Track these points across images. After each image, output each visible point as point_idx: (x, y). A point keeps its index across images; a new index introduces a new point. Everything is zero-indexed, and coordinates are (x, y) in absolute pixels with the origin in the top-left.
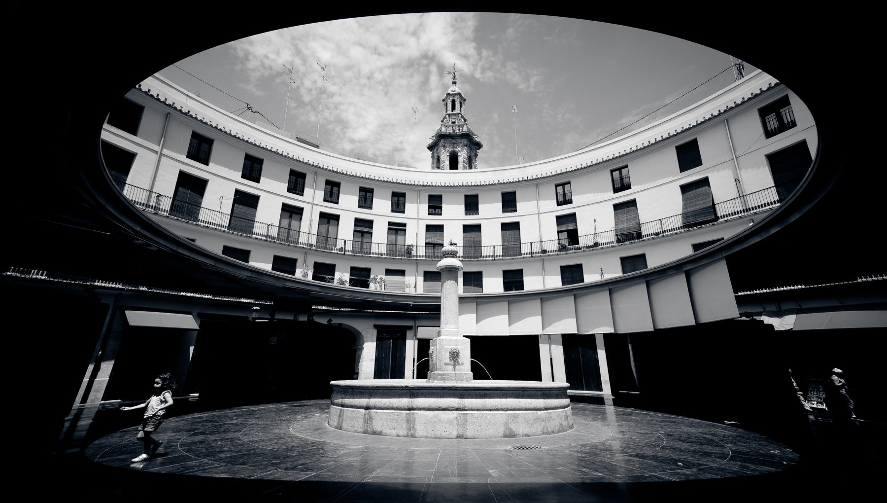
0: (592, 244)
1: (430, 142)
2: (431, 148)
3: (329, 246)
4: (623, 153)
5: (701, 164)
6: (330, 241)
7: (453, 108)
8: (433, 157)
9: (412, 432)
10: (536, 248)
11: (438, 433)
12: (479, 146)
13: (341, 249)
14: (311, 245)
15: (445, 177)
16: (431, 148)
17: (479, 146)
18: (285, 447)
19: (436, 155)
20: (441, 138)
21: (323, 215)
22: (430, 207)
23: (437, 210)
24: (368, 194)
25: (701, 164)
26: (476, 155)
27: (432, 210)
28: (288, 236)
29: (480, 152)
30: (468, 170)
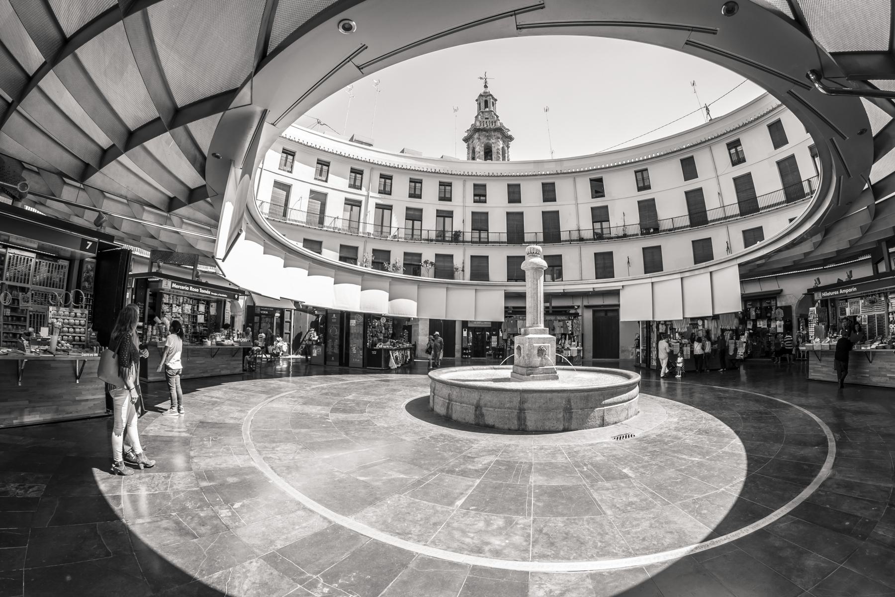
0: (621, 234)
1: (466, 134)
2: (466, 140)
3: (384, 234)
4: (313, 145)
5: (787, 143)
6: (385, 229)
7: (486, 106)
8: (468, 148)
9: (523, 427)
10: (575, 236)
11: (547, 428)
12: (511, 138)
13: (395, 237)
14: (369, 234)
15: (481, 167)
16: (466, 140)
17: (511, 138)
18: (288, 543)
19: (471, 146)
20: (475, 130)
21: (378, 206)
22: (475, 195)
23: (482, 198)
24: (418, 185)
25: (787, 143)
26: (508, 147)
27: (477, 198)
28: (353, 225)
29: (511, 144)
30: (471, 161)
